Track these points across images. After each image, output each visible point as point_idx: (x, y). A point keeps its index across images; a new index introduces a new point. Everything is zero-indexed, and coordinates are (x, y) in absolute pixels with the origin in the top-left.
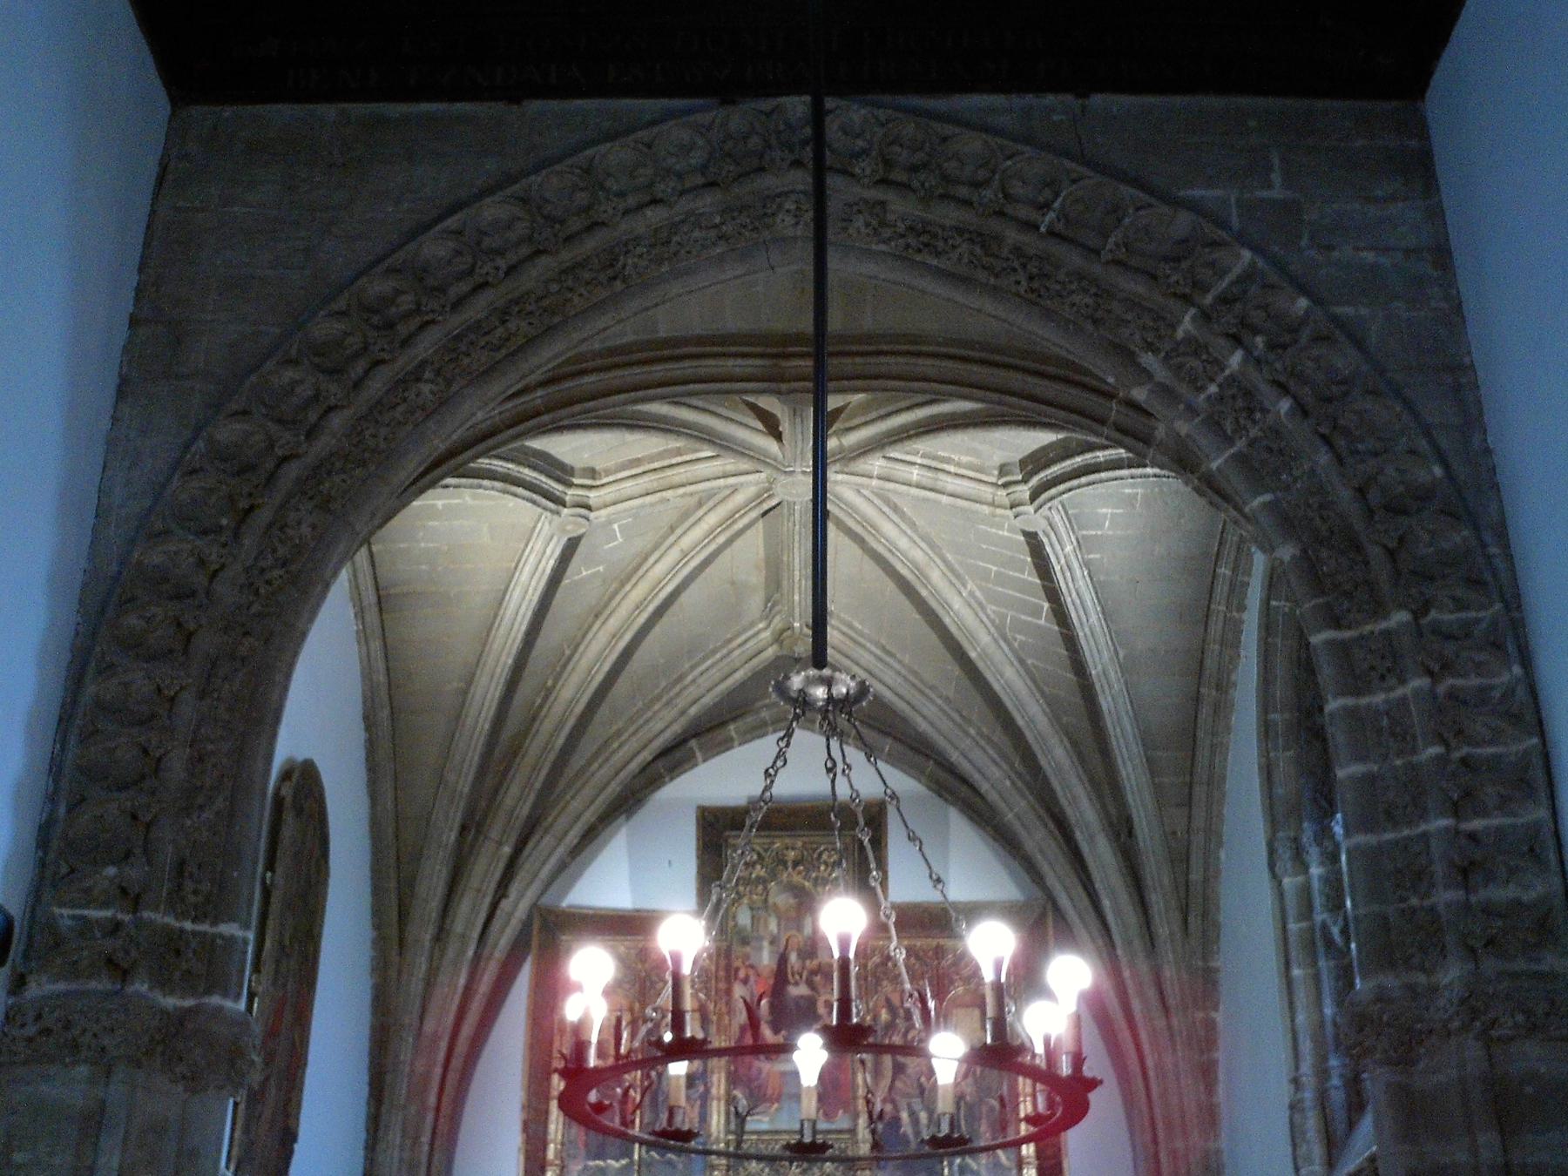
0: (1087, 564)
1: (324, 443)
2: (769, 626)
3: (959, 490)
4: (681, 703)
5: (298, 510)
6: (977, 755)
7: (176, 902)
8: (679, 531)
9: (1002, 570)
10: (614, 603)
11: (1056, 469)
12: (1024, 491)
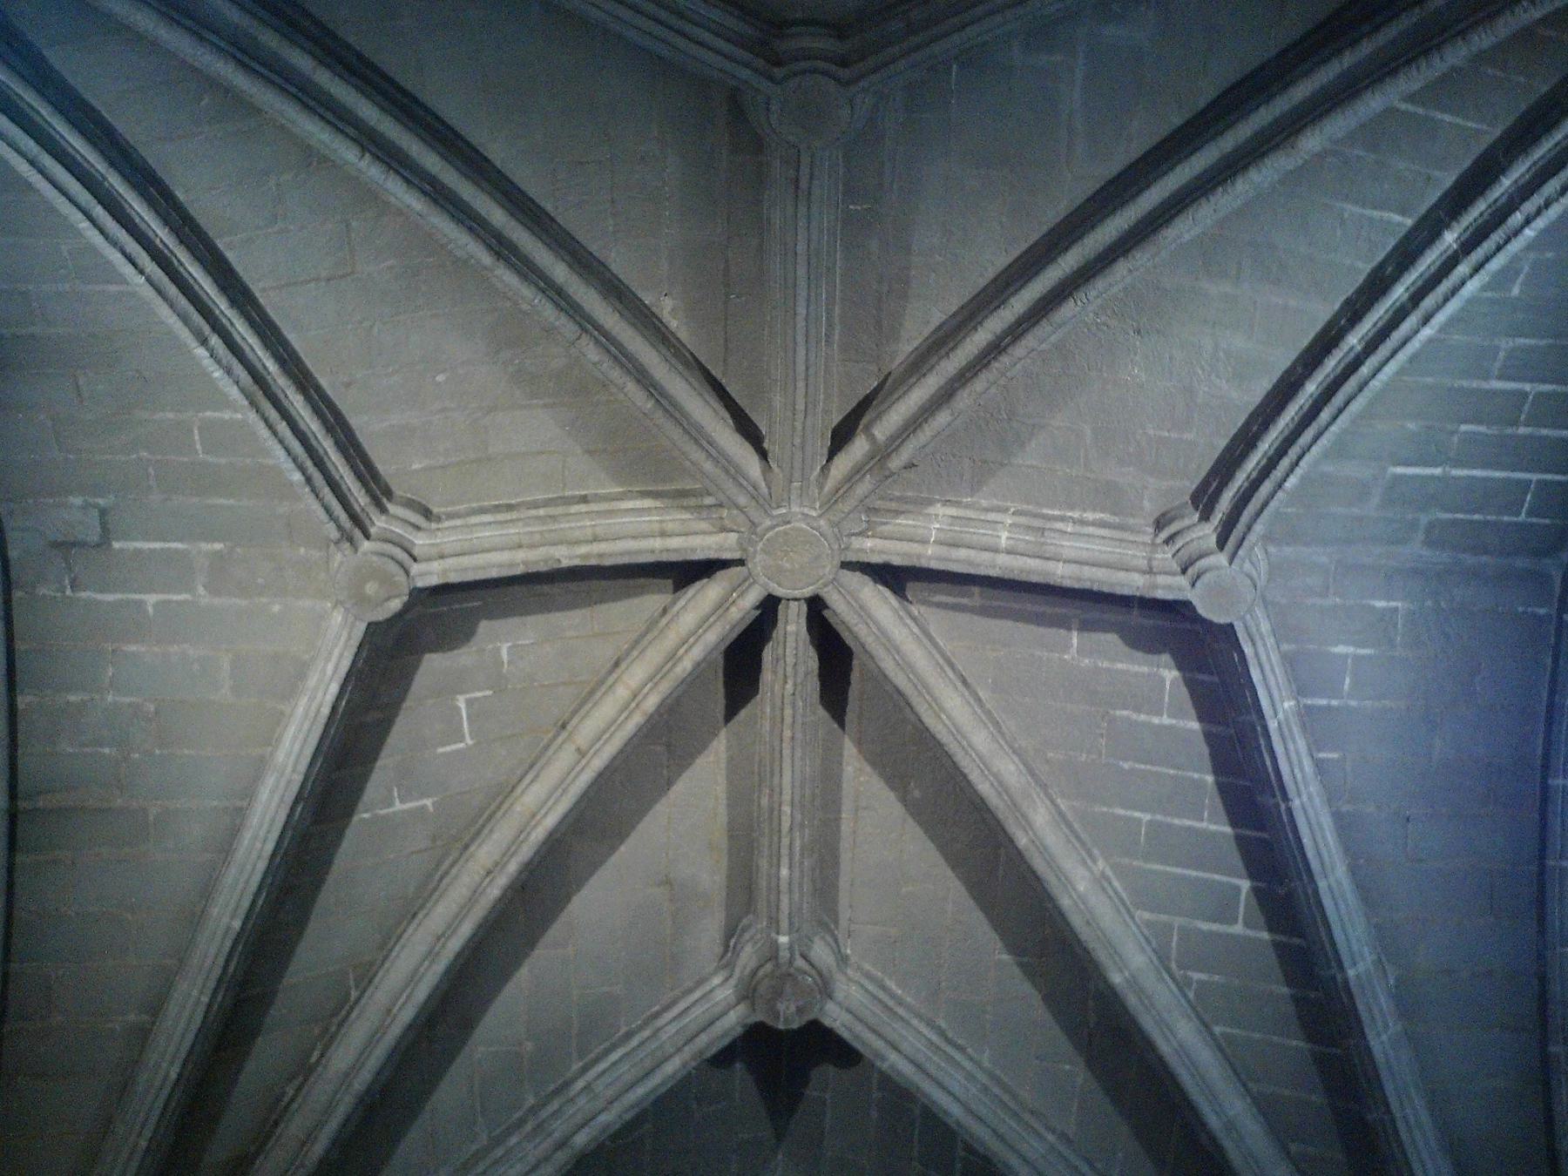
4: (559, 1129)
9: (1159, 817)
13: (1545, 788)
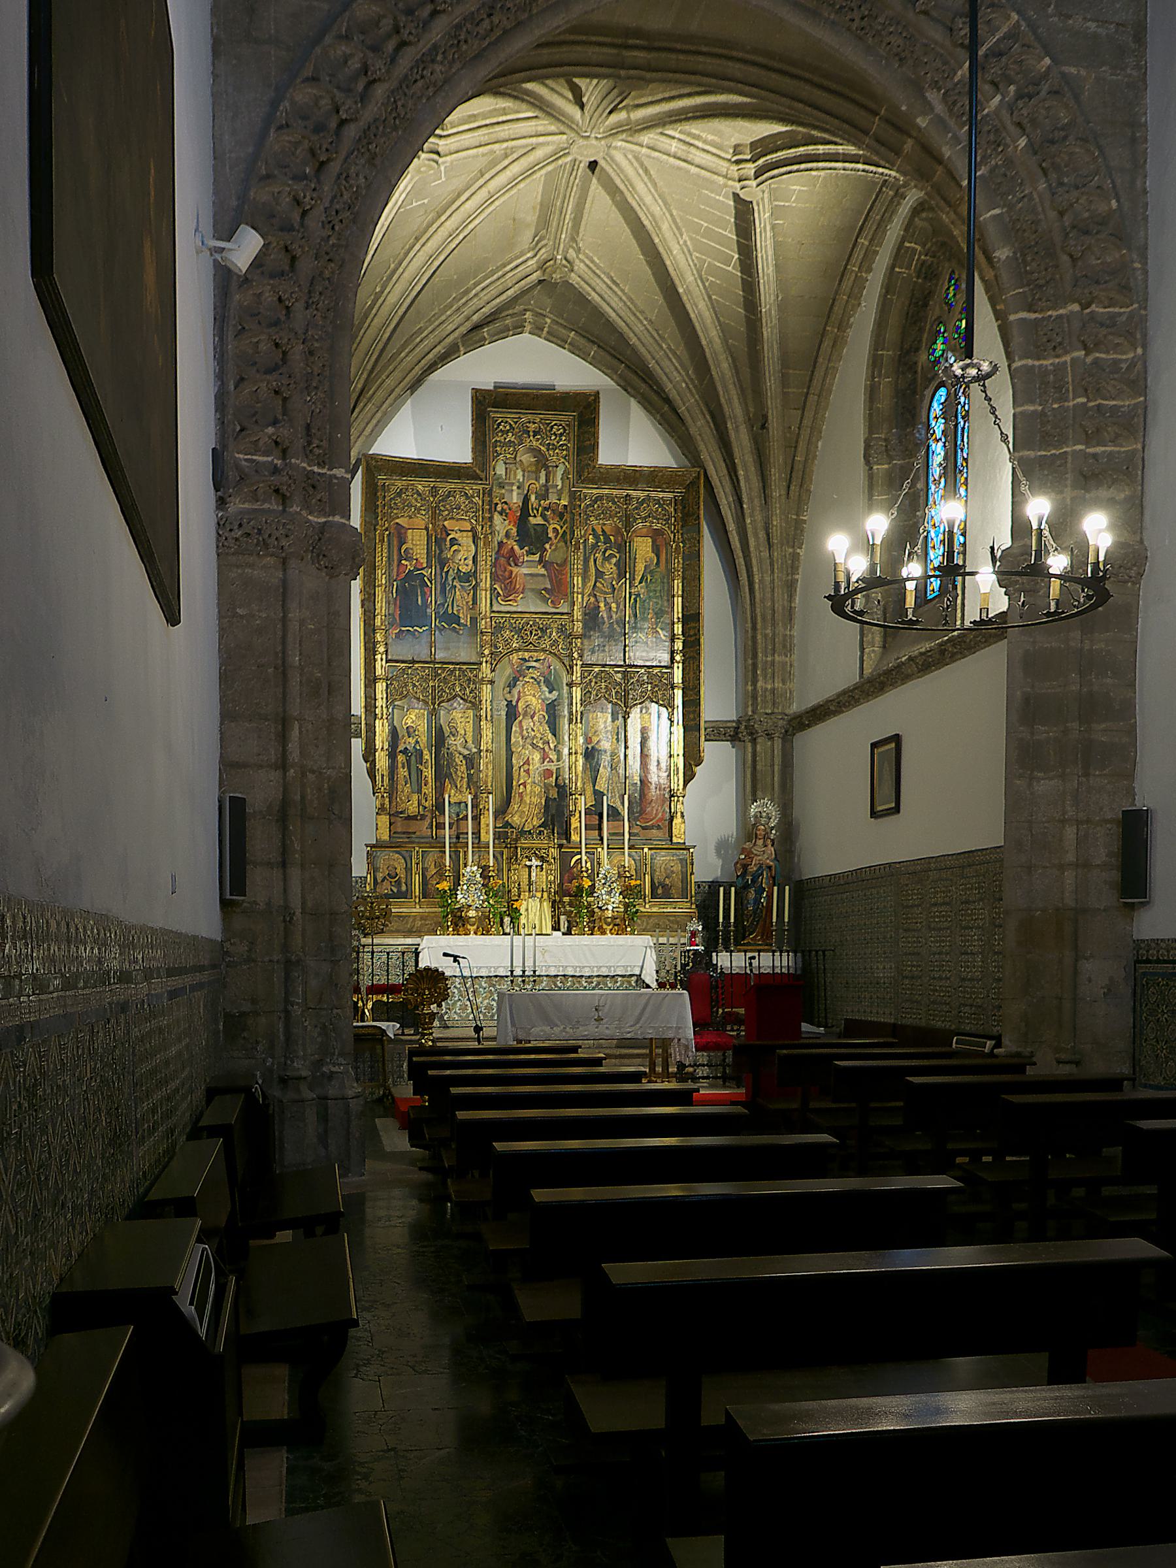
0: (773, 227)
1: (370, 112)
2: (535, 255)
3: (703, 162)
4: (467, 311)
5: (356, 164)
6: (665, 363)
7: (307, 453)
8: (487, 176)
10: (432, 230)
11: (781, 154)
12: (750, 169)
13: (824, 329)
